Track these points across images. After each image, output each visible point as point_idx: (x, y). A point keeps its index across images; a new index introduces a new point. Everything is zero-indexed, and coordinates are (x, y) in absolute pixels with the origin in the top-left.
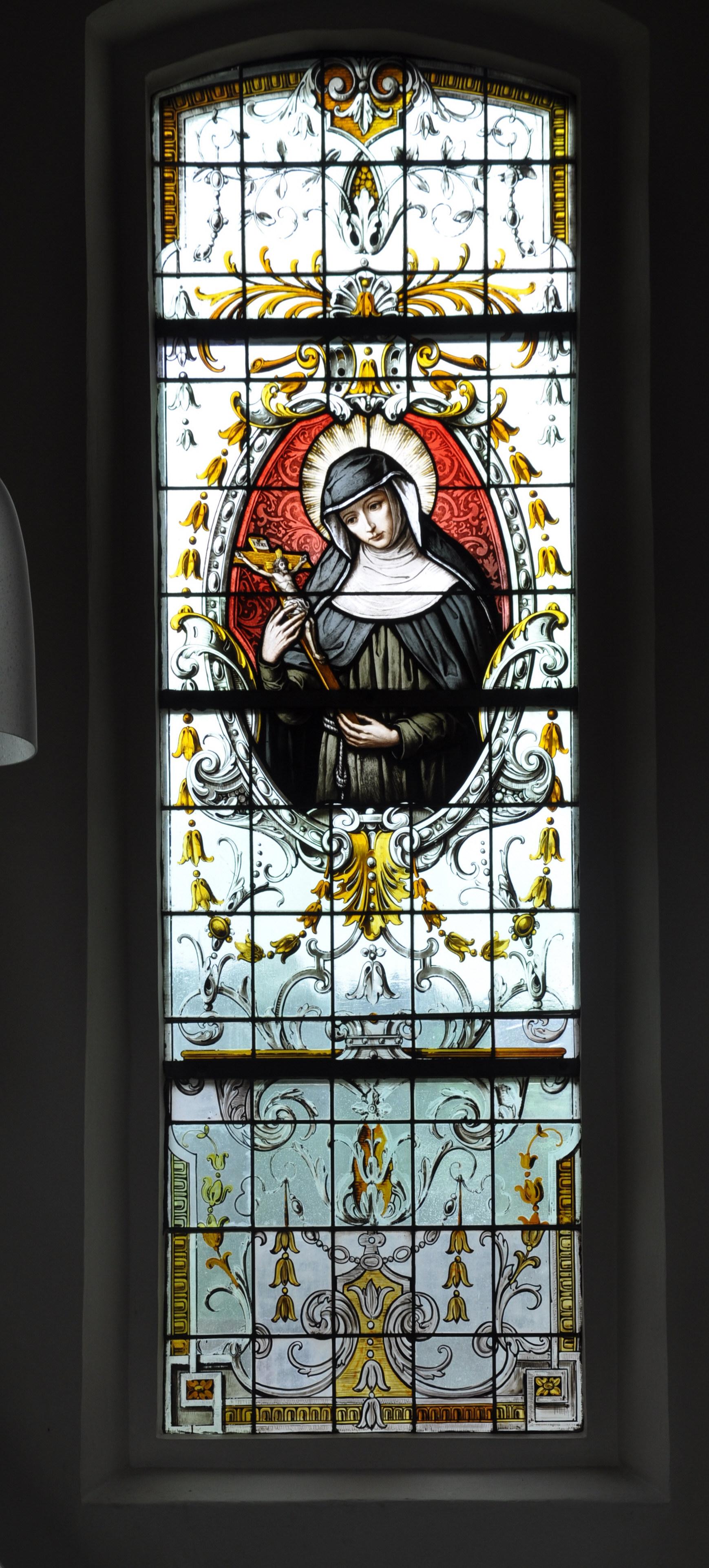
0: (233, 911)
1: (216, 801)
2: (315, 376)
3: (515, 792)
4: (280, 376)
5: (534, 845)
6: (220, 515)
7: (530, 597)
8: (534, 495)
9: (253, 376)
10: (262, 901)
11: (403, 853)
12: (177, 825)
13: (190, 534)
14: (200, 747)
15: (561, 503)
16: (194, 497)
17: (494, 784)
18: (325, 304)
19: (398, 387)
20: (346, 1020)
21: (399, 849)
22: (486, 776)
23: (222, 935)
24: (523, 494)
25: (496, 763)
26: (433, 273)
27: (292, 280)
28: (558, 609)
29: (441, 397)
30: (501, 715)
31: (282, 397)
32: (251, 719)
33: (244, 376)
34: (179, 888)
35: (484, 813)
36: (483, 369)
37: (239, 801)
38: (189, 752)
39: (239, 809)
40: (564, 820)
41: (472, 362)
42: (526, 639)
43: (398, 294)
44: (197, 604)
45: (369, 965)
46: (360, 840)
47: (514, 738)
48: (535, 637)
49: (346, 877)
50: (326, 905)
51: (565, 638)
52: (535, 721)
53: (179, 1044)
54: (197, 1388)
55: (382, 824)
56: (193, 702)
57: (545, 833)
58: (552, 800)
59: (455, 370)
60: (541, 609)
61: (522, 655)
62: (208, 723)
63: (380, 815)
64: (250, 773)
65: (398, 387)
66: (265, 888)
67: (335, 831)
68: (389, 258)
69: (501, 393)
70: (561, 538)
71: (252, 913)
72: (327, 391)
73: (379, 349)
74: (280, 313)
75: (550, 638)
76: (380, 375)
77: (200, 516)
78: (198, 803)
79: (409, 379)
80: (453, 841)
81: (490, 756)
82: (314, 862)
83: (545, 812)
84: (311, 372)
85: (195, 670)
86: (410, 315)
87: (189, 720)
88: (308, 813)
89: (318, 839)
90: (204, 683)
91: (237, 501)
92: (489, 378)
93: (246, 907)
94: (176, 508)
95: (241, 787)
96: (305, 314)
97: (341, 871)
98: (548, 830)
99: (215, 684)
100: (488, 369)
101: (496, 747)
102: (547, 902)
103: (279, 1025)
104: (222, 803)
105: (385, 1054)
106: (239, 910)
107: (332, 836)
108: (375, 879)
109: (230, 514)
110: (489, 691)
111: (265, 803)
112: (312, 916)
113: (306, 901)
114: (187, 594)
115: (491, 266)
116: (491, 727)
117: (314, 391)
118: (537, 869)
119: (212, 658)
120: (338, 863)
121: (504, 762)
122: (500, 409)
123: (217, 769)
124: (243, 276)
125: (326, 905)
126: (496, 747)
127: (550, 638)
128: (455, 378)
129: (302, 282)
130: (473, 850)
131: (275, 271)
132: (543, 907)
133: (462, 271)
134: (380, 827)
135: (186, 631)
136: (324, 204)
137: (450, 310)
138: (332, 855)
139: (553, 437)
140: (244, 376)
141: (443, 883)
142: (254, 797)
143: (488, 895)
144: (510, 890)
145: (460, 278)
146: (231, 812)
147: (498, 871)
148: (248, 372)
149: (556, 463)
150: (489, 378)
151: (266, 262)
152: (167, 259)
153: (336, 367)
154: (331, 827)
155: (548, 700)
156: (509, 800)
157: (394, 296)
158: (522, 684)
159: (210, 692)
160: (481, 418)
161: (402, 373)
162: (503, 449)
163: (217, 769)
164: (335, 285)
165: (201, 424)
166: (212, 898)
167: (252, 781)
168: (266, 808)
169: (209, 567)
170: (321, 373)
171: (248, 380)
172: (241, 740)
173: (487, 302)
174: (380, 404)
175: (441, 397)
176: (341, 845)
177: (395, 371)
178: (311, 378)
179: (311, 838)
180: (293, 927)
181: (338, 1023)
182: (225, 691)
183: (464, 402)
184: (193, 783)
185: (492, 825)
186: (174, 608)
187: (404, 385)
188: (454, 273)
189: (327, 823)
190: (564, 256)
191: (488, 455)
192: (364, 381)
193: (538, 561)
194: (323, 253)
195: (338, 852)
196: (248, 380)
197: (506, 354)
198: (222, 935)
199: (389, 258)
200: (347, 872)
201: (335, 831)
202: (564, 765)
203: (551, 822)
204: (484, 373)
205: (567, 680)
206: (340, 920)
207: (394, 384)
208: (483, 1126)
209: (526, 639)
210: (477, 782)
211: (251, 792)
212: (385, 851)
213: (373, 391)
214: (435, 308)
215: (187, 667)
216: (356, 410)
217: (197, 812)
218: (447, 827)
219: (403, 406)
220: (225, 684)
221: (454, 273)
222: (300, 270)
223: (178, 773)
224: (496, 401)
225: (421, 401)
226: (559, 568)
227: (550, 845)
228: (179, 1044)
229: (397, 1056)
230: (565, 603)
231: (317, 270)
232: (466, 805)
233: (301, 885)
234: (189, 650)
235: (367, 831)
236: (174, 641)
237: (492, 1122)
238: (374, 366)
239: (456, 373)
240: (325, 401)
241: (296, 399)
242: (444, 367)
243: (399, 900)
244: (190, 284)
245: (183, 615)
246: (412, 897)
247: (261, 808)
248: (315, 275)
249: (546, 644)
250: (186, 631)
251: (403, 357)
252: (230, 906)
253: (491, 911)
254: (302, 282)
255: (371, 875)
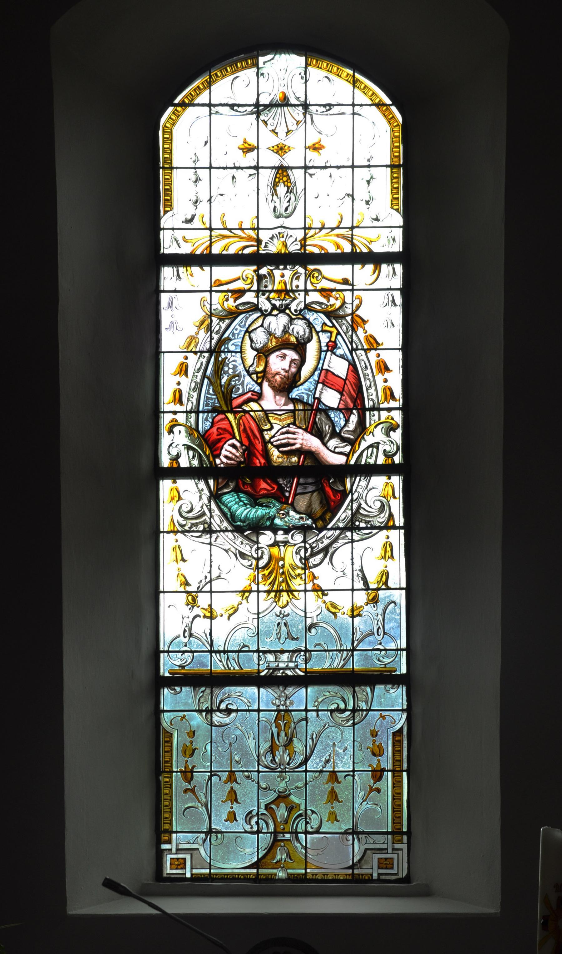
0: (199, 591)
1: (190, 528)
2: (252, 289)
3: (367, 522)
4: (230, 289)
5: (379, 551)
6: (190, 389)
7: (376, 413)
8: (379, 355)
9: (213, 289)
10: (216, 586)
11: (301, 559)
12: (167, 543)
13: (177, 379)
14: (180, 498)
15: (395, 360)
16: (180, 358)
17: (355, 515)
18: (258, 246)
19: (299, 294)
20: (265, 652)
21: (298, 556)
22: (349, 512)
23: (193, 603)
24: (372, 355)
25: (355, 506)
26: (321, 229)
27: (239, 232)
28: (392, 419)
29: (324, 301)
30: (358, 478)
31: (231, 300)
32: (211, 482)
33: (209, 289)
34: (169, 578)
35: (349, 534)
36: (350, 285)
37: (204, 527)
38: (176, 499)
39: (204, 531)
40: (397, 538)
41: (342, 281)
42: (374, 436)
43: (300, 241)
44: (181, 418)
45: (279, 621)
46: (275, 550)
47: (366, 492)
48: (378, 435)
49: (266, 572)
50: (254, 587)
51: (397, 436)
52: (378, 481)
53: (168, 665)
54: (176, 863)
55: (288, 542)
56: (176, 473)
57: (384, 545)
58: (388, 526)
59: (332, 286)
60: (383, 419)
61: (371, 446)
62: (187, 485)
63: (287, 536)
64: (210, 510)
65: (299, 294)
66: (219, 577)
67: (260, 545)
68: (296, 220)
69: (358, 298)
70: (395, 380)
71: (211, 592)
72: (257, 297)
73: (288, 273)
74: (232, 250)
75: (388, 435)
76: (288, 289)
77: (183, 370)
78: (180, 529)
79: (306, 291)
80: (331, 550)
81: (352, 501)
82: (246, 563)
83: (384, 533)
84: (249, 286)
85: (178, 456)
86: (307, 252)
87: (175, 482)
88: (246, 534)
89: (249, 548)
90: (184, 463)
91: (204, 361)
92: (352, 290)
93: (207, 588)
94: (169, 364)
95: (205, 520)
96: (246, 251)
97: (264, 568)
98: (387, 542)
99: (190, 462)
100: (353, 285)
101: (355, 496)
102: (386, 583)
103: (226, 655)
104: (194, 529)
105: (289, 673)
106: (203, 590)
107: (258, 548)
108: (283, 566)
109: (199, 369)
110: (352, 465)
111: (219, 529)
112: (245, 592)
113: (243, 584)
114: (175, 413)
115: (355, 225)
116: (352, 486)
117: (249, 297)
118: (380, 566)
119: (189, 448)
120: (262, 563)
121: (359, 507)
122: (358, 307)
123: (191, 510)
124: (211, 229)
125: (254, 587)
126: (355, 496)
127: (388, 435)
128: (332, 290)
129: (245, 234)
130: (342, 554)
131: (228, 227)
132: (384, 587)
133: (338, 227)
134: (286, 543)
135: (173, 433)
136: (258, 189)
137: (332, 250)
138: (258, 559)
139: (390, 324)
140: (209, 289)
141: (325, 574)
142: (212, 526)
143: (351, 581)
144: (364, 579)
145: (337, 232)
146: (199, 534)
147: (357, 566)
148: (211, 287)
149: (392, 337)
150: (352, 290)
151: (223, 222)
152: (166, 221)
153: (264, 282)
154: (257, 542)
155: (387, 470)
156: (363, 525)
157: (299, 243)
158: (372, 461)
159: (187, 468)
160: (349, 311)
161: (302, 287)
162: (360, 332)
163: (191, 510)
164: (264, 236)
165: (184, 310)
166: (187, 584)
167: (211, 516)
168: (219, 531)
169: (188, 398)
170: (255, 287)
171: (211, 291)
172: (206, 492)
173: (353, 245)
174: (289, 304)
175: (324, 301)
176: (263, 553)
177: (297, 286)
178: (249, 290)
179: (246, 549)
180: (235, 599)
181: (261, 654)
182: (195, 467)
183: (338, 304)
184: (177, 517)
185: (352, 541)
186: (166, 420)
187: (303, 294)
188: (333, 229)
189: (255, 540)
190: (398, 220)
191: (352, 335)
192: (279, 292)
193: (381, 394)
194: (257, 217)
195: (262, 557)
196: (211, 291)
197: (363, 274)
198: (193, 603)
199: (296, 220)
200: (267, 570)
201: (260, 545)
202: (397, 507)
203: (388, 538)
204: (350, 287)
205: (398, 459)
206: (263, 595)
207: (297, 294)
208: (348, 713)
209: (374, 436)
210: (343, 517)
211: (211, 522)
212: (291, 557)
213: (285, 297)
214: (322, 248)
215: (174, 452)
216: (274, 307)
217: (179, 534)
218: (326, 542)
219: (302, 306)
220: (195, 463)
221: (333, 229)
222: (243, 227)
223: (168, 513)
224: (357, 302)
225: (313, 303)
226: (393, 397)
227: (388, 552)
228: (168, 665)
229: (296, 673)
230: (397, 416)
231: (253, 226)
232: (338, 528)
233: (239, 575)
234: (174, 445)
235: (279, 546)
236: (166, 440)
237: (354, 711)
238: (285, 283)
239: (333, 288)
240: (256, 303)
241: (239, 302)
242: (325, 284)
243: (297, 584)
244: (179, 234)
245: (173, 423)
246: (305, 584)
247: (216, 531)
248: (253, 229)
249: (386, 439)
250: (173, 433)
251: (302, 278)
252: (198, 588)
253: (353, 590)
254: (245, 234)
255: (281, 571)
